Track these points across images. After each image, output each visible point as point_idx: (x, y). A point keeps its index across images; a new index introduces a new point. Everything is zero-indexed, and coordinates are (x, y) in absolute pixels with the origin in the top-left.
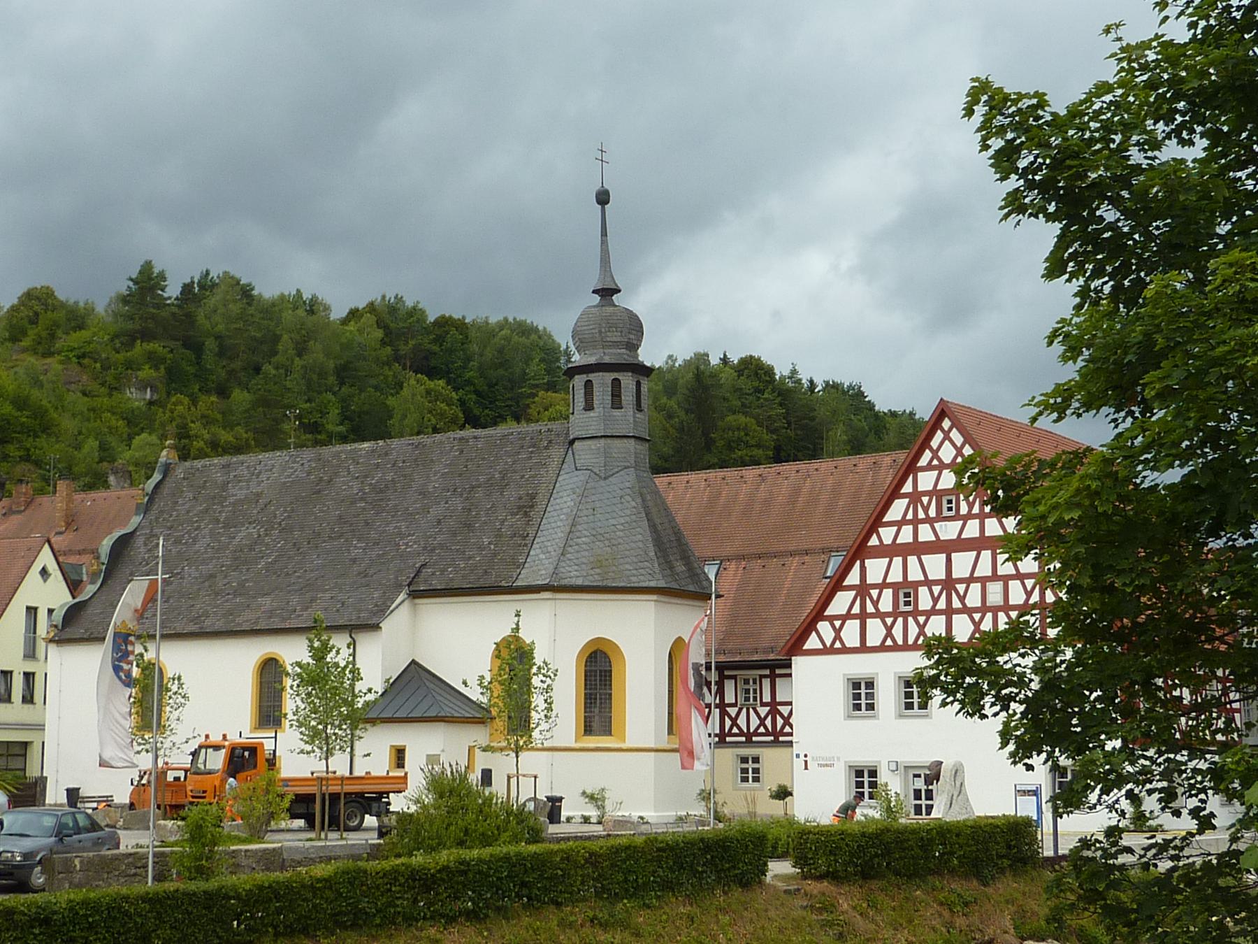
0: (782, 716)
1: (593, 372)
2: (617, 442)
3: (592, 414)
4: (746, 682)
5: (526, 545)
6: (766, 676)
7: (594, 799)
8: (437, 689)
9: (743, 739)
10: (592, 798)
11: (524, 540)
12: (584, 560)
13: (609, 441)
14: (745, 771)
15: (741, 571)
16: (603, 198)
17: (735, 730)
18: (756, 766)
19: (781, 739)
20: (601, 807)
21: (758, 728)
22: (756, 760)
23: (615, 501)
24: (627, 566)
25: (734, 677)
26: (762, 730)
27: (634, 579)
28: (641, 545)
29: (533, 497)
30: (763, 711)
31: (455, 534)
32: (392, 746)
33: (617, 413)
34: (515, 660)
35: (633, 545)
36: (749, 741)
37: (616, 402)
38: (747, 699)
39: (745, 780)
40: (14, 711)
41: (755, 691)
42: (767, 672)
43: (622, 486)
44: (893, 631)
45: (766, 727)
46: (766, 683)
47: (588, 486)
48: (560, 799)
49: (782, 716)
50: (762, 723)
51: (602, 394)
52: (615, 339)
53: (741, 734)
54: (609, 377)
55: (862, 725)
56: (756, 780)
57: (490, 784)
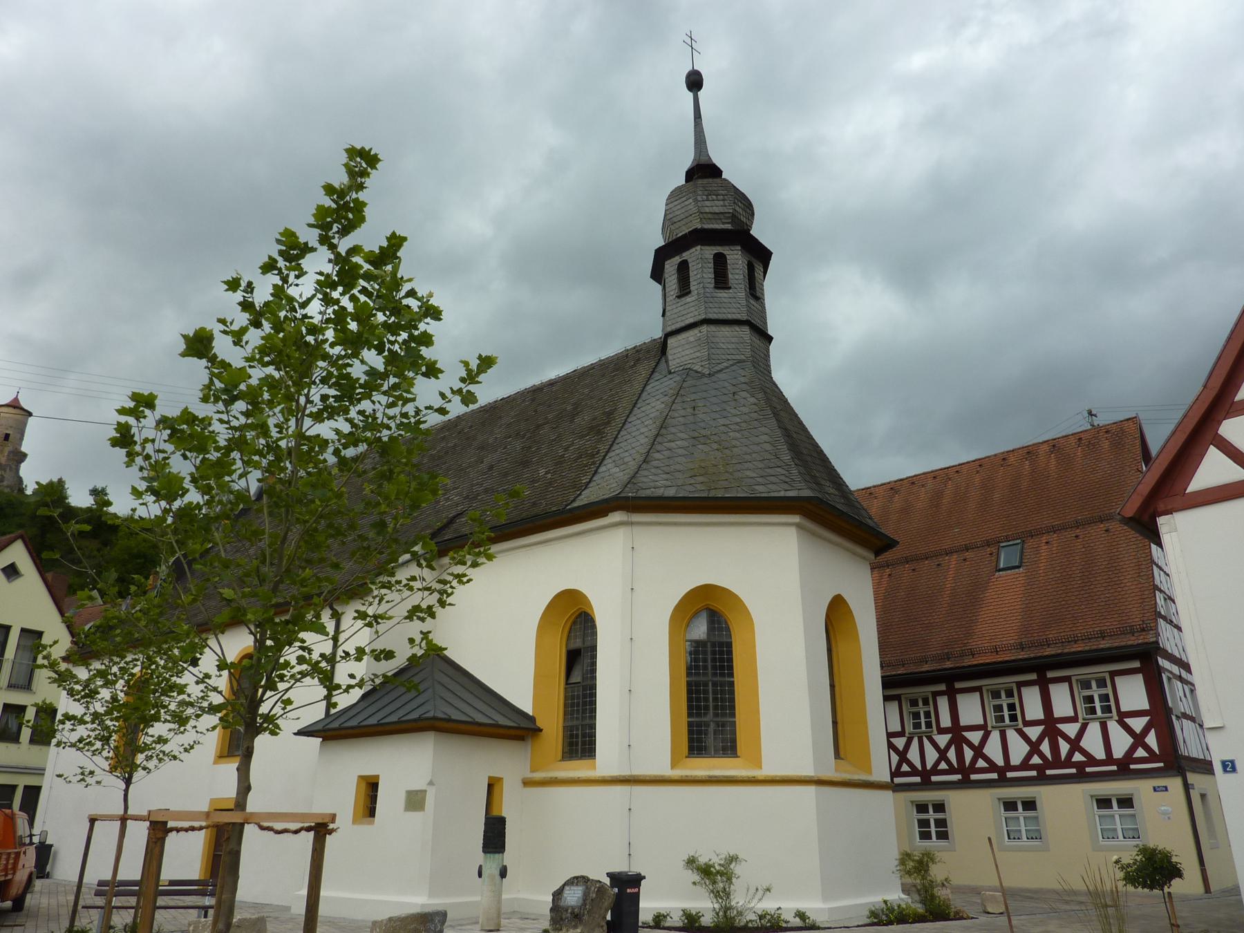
0: (970, 745)
1: (687, 248)
2: (725, 331)
3: (688, 299)
4: (914, 703)
5: (594, 463)
6: (941, 693)
7: (713, 875)
8: (446, 680)
9: (918, 779)
10: (706, 872)
11: (593, 461)
12: (678, 467)
13: (713, 328)
14: (924, 823)
15: (886, 578)
16: (695, 82)
17: (905, 768)
18: (940, 816)
19: (974, 777)
20: (722, 895)
21: (937, 763)
22: (939, 807)
23: (725, 398)
24: (748, 473)
25: (1067, 679)
26: (943, 766)
27: (760, 488)
28: (768, 447)
29: (610, 415)
30: (942, 740)
31: (506, 475)
32: (361, 777)
33: (722, 294)
34: (574, 635)
35: (755, 448)
36: (926, 784)
37: (721, 281)
38: (917, 726)
39: (925, 836)
40: (19, 753)
41: (927, 715)
42: (943, 687)
43: (734, 382)
44: (909, 756)
45: (948, 762)
46: (943, 703)
47: (685, 385)
48: (637, 880)
49: (970, 745)
50: (943, 754)
52: (716, 210)
53: (914, 772)
54: (709, 252)
56: (943, 836)
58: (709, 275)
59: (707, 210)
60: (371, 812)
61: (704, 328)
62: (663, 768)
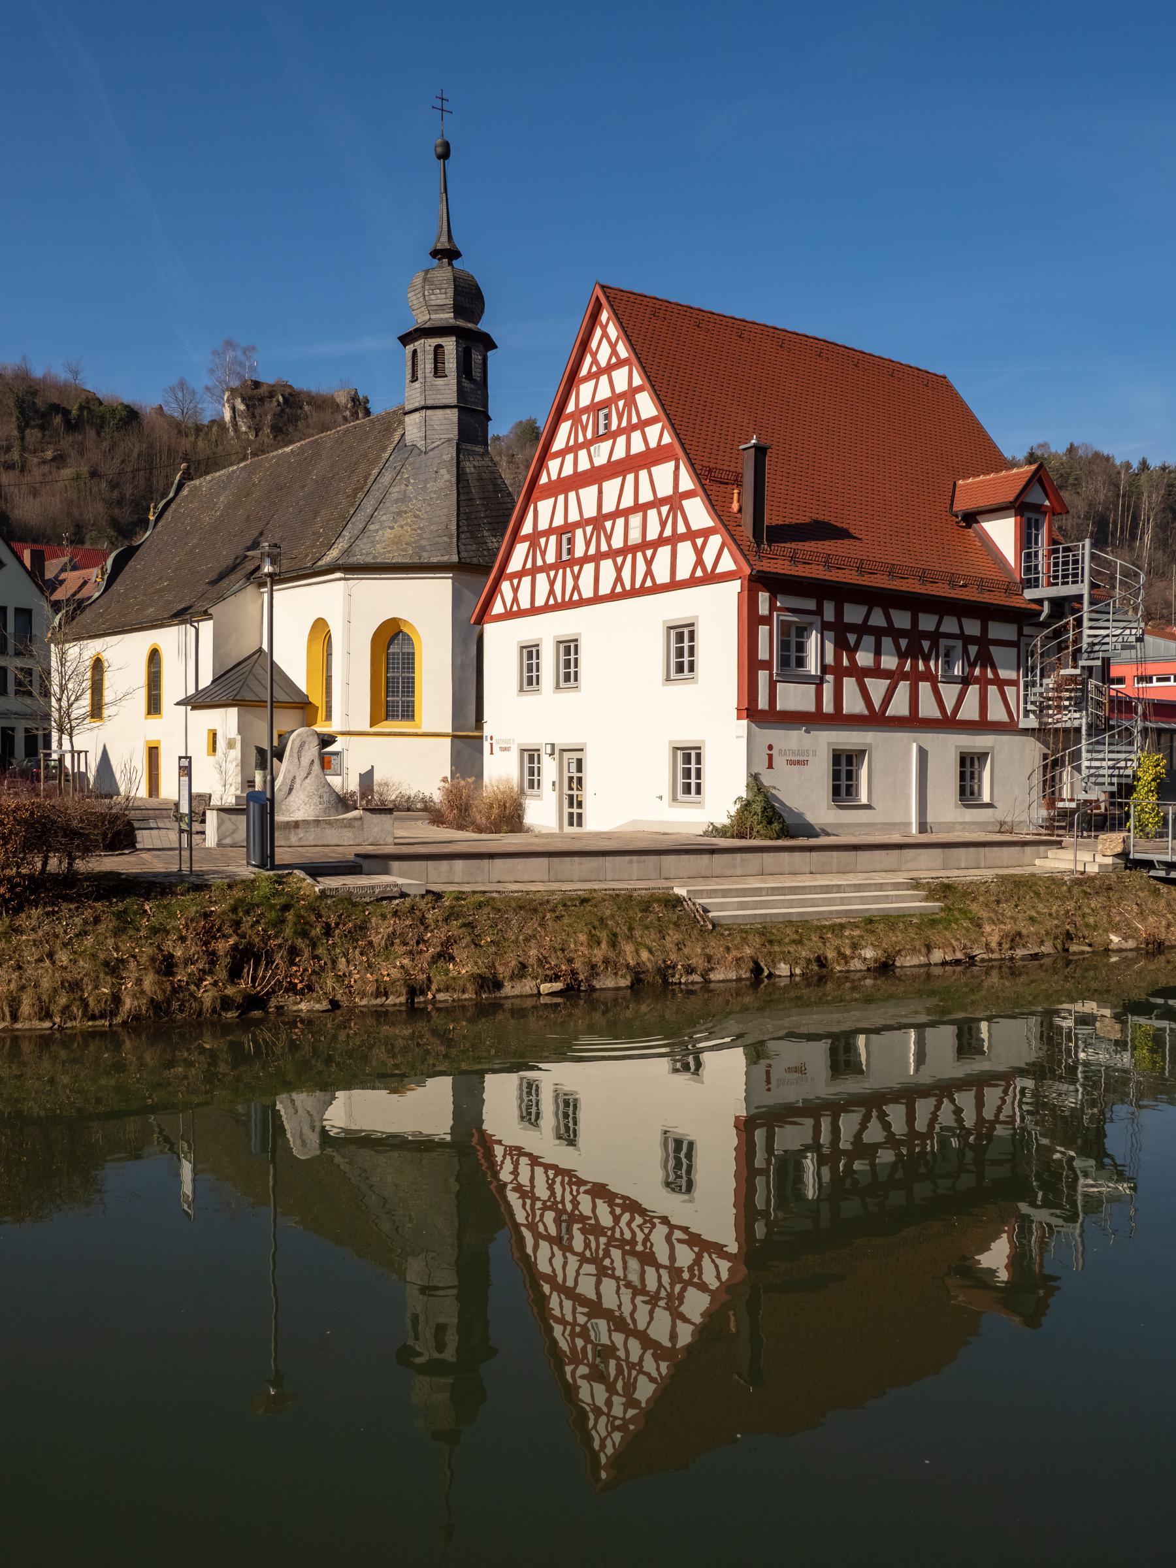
2: (439, 412)
3: (417, 385)
13: (429, 412)
33: (440, 382)
37: (438, 372)
51: (426, 365)
52: (440, 302)
55: (154, 721)
57: (157, 796)
58: (430, 366)
59: (433, 303)
60: (214, 750)
61: (423, 412)
62: (366, 727)
